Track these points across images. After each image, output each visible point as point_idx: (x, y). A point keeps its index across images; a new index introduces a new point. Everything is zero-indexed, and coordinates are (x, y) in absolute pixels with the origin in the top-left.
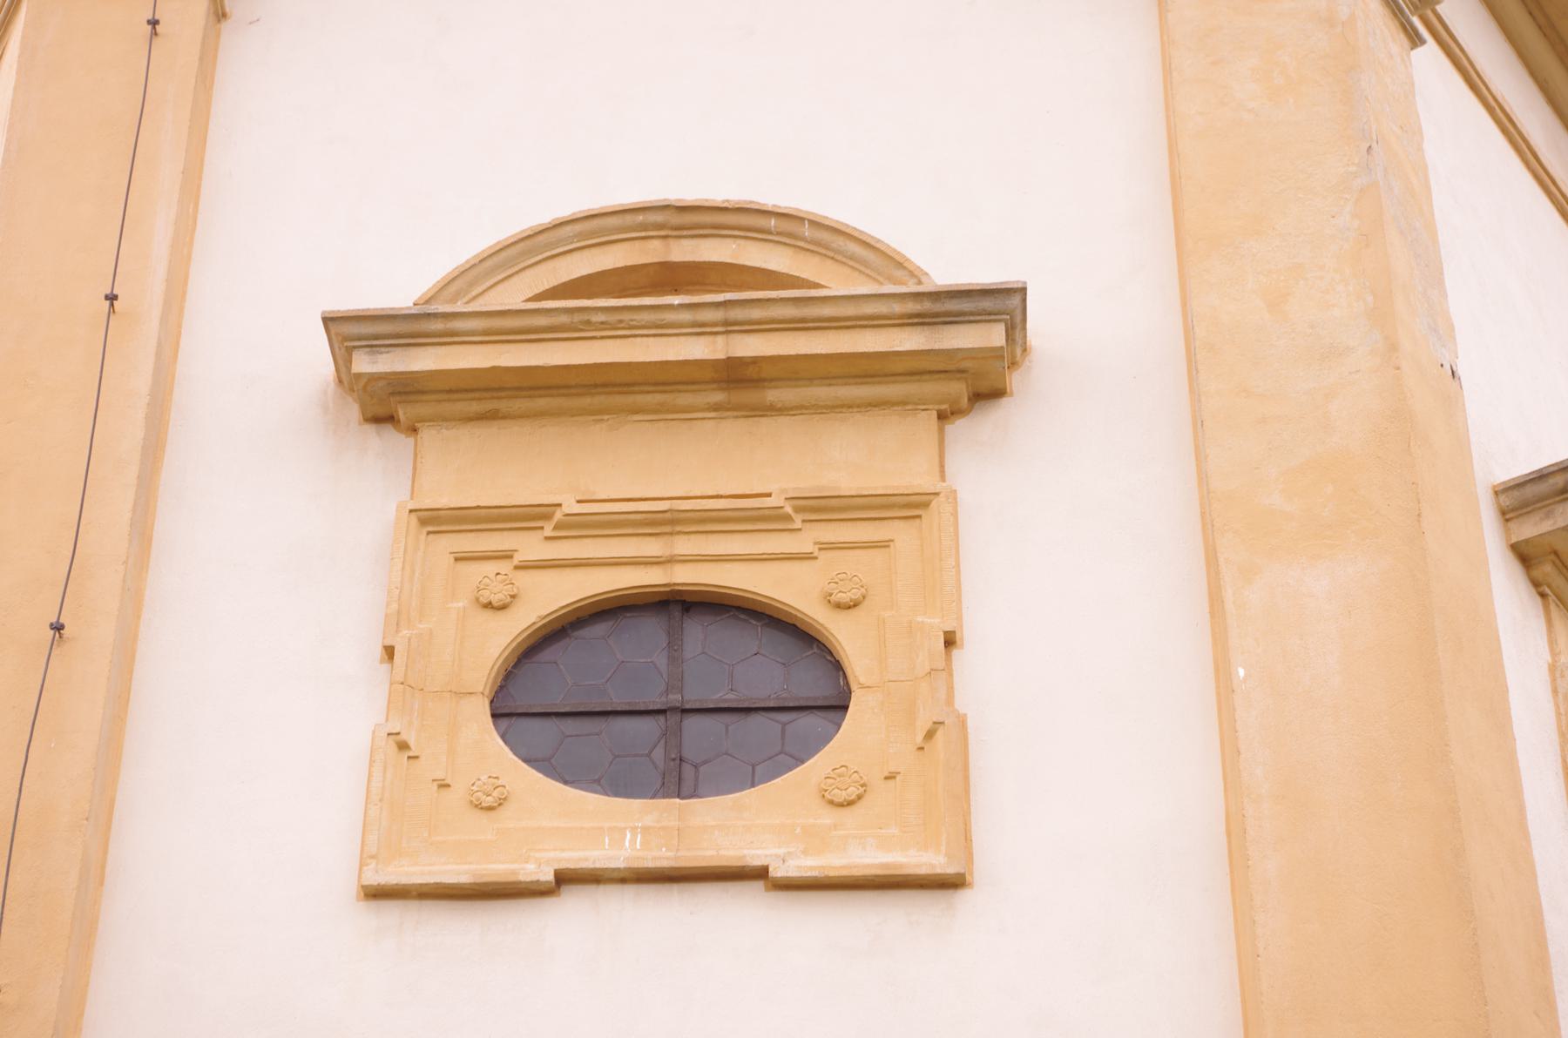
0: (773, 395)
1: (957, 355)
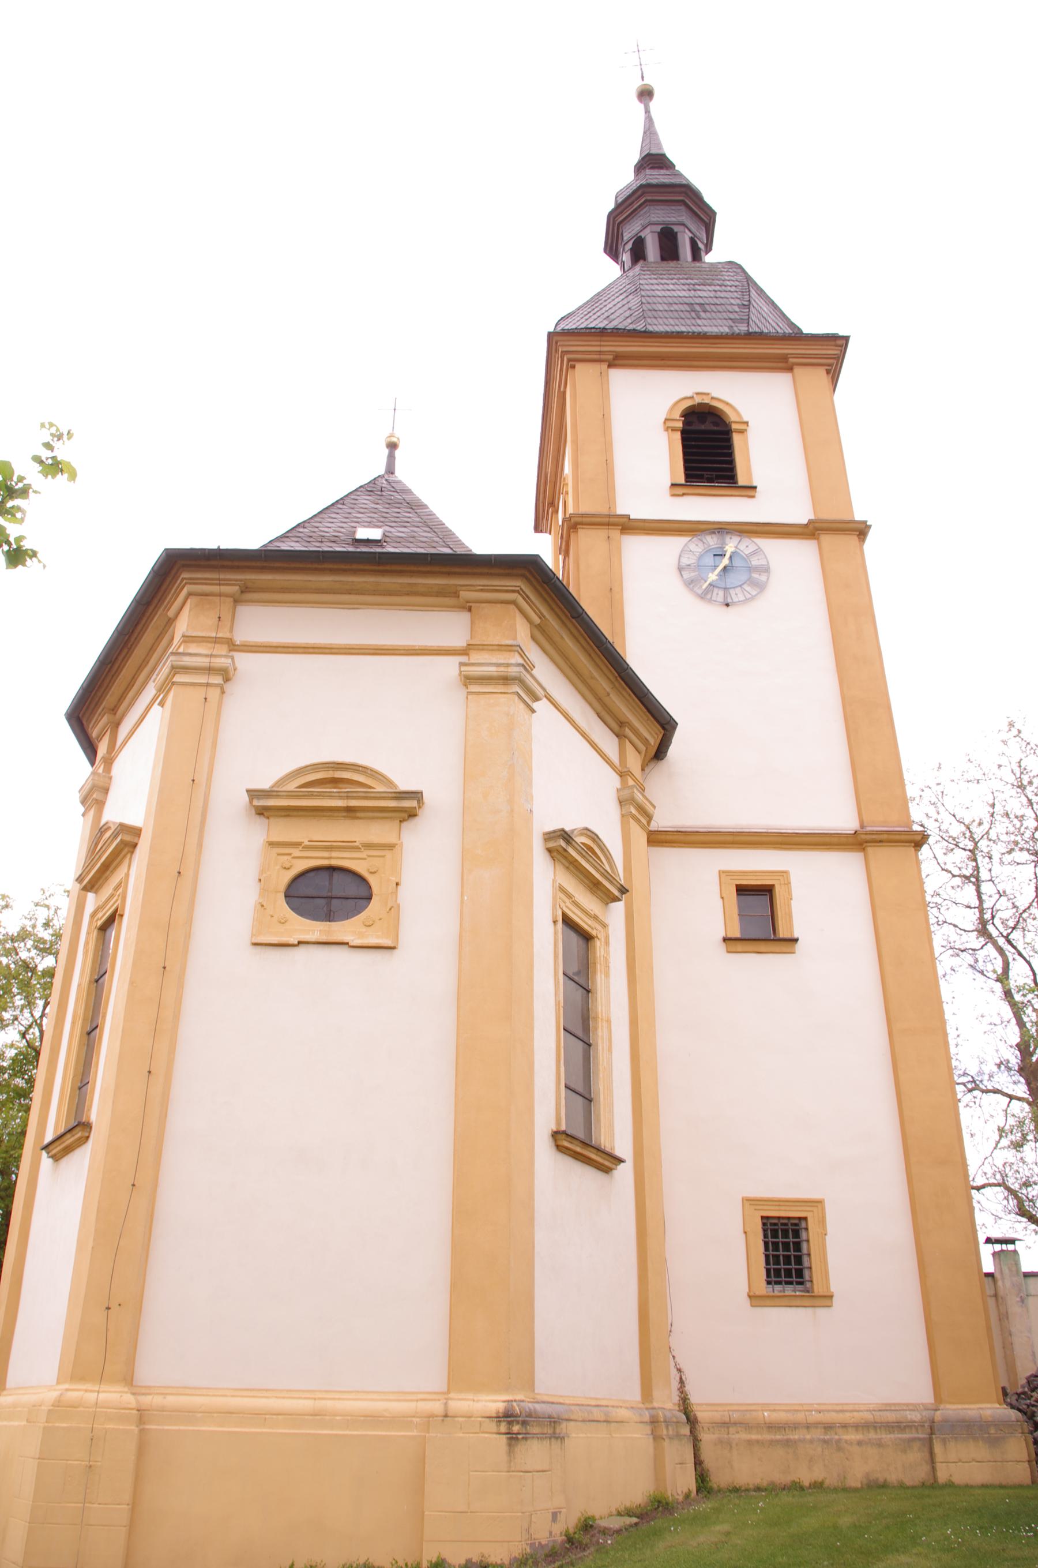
0: (358, 814)
1: (406, 807)
